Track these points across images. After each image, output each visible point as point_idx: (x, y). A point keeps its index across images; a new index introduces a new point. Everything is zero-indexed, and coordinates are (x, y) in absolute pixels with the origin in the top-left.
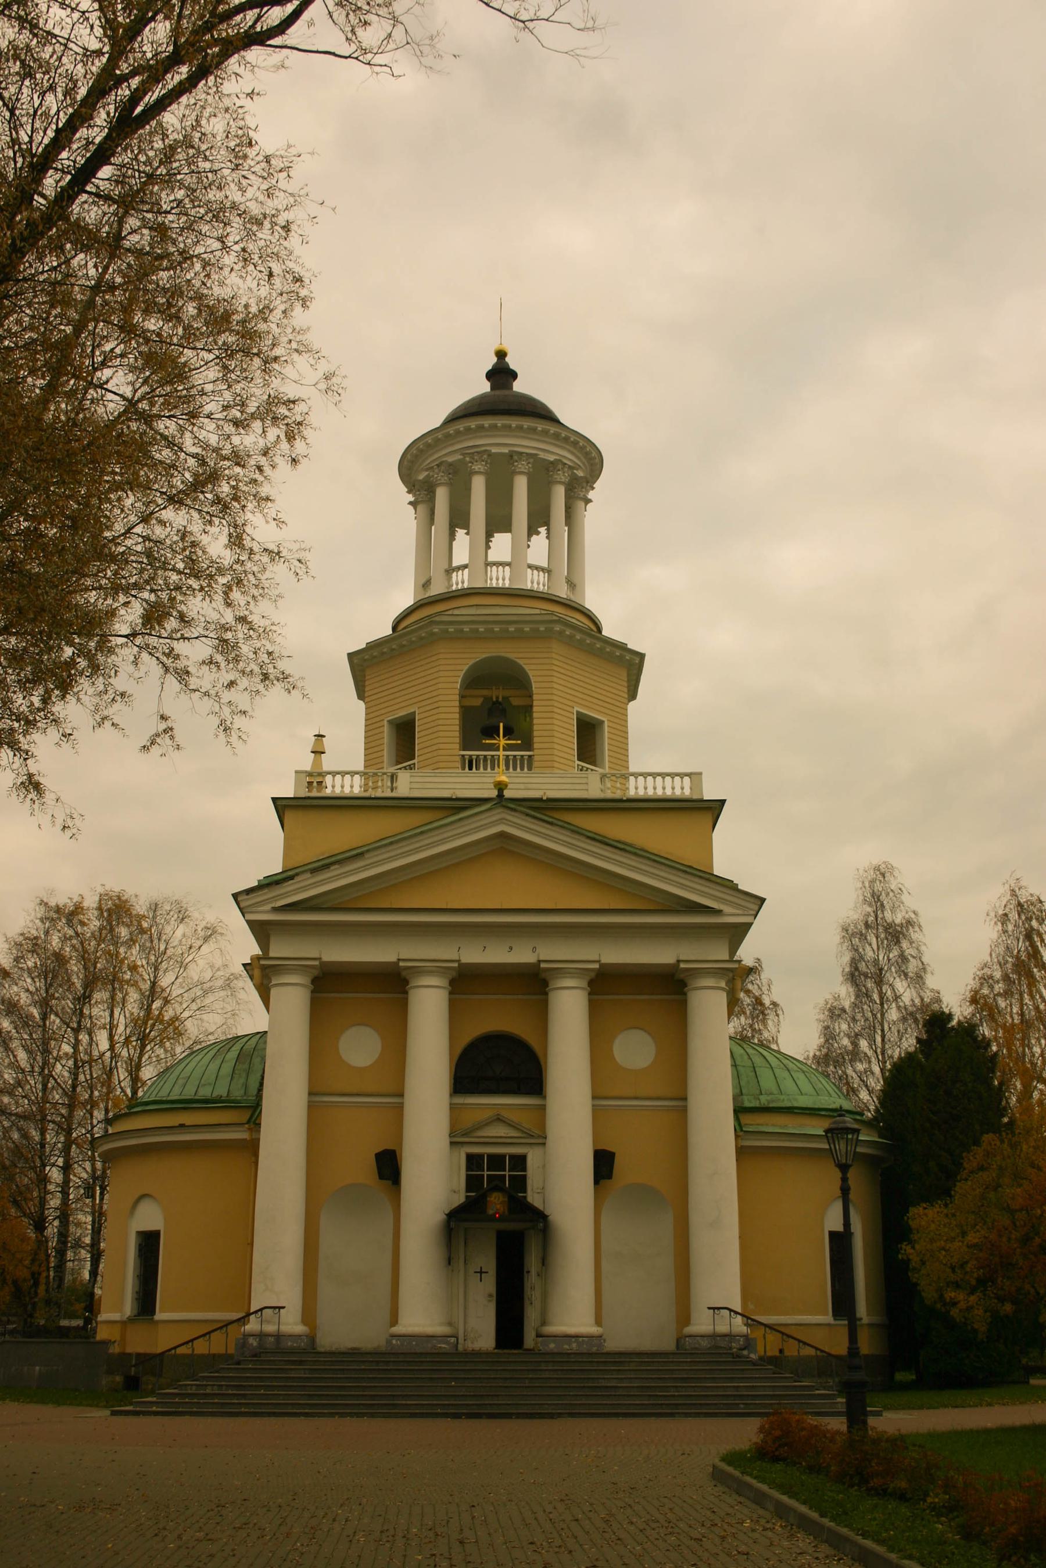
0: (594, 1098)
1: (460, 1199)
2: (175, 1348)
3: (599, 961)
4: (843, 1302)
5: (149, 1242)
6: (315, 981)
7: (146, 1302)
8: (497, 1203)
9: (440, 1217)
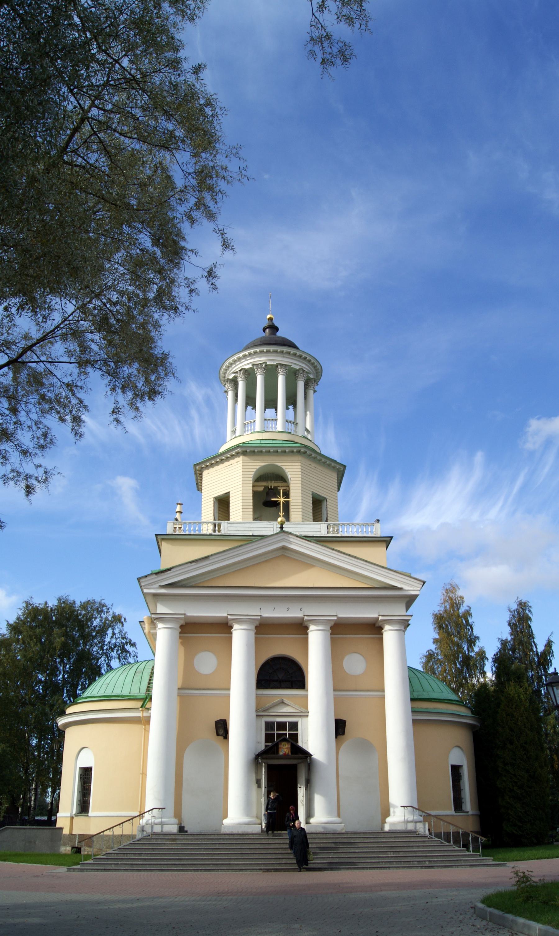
0: (334, 690)
1: (262, 747)
2: (103, 832)
3: (336, 616)
4: (458, 804)
5: (86, 774)
6: (182, 627)
7: (84, 807)
8: (285, 749)
9: (254, 756)
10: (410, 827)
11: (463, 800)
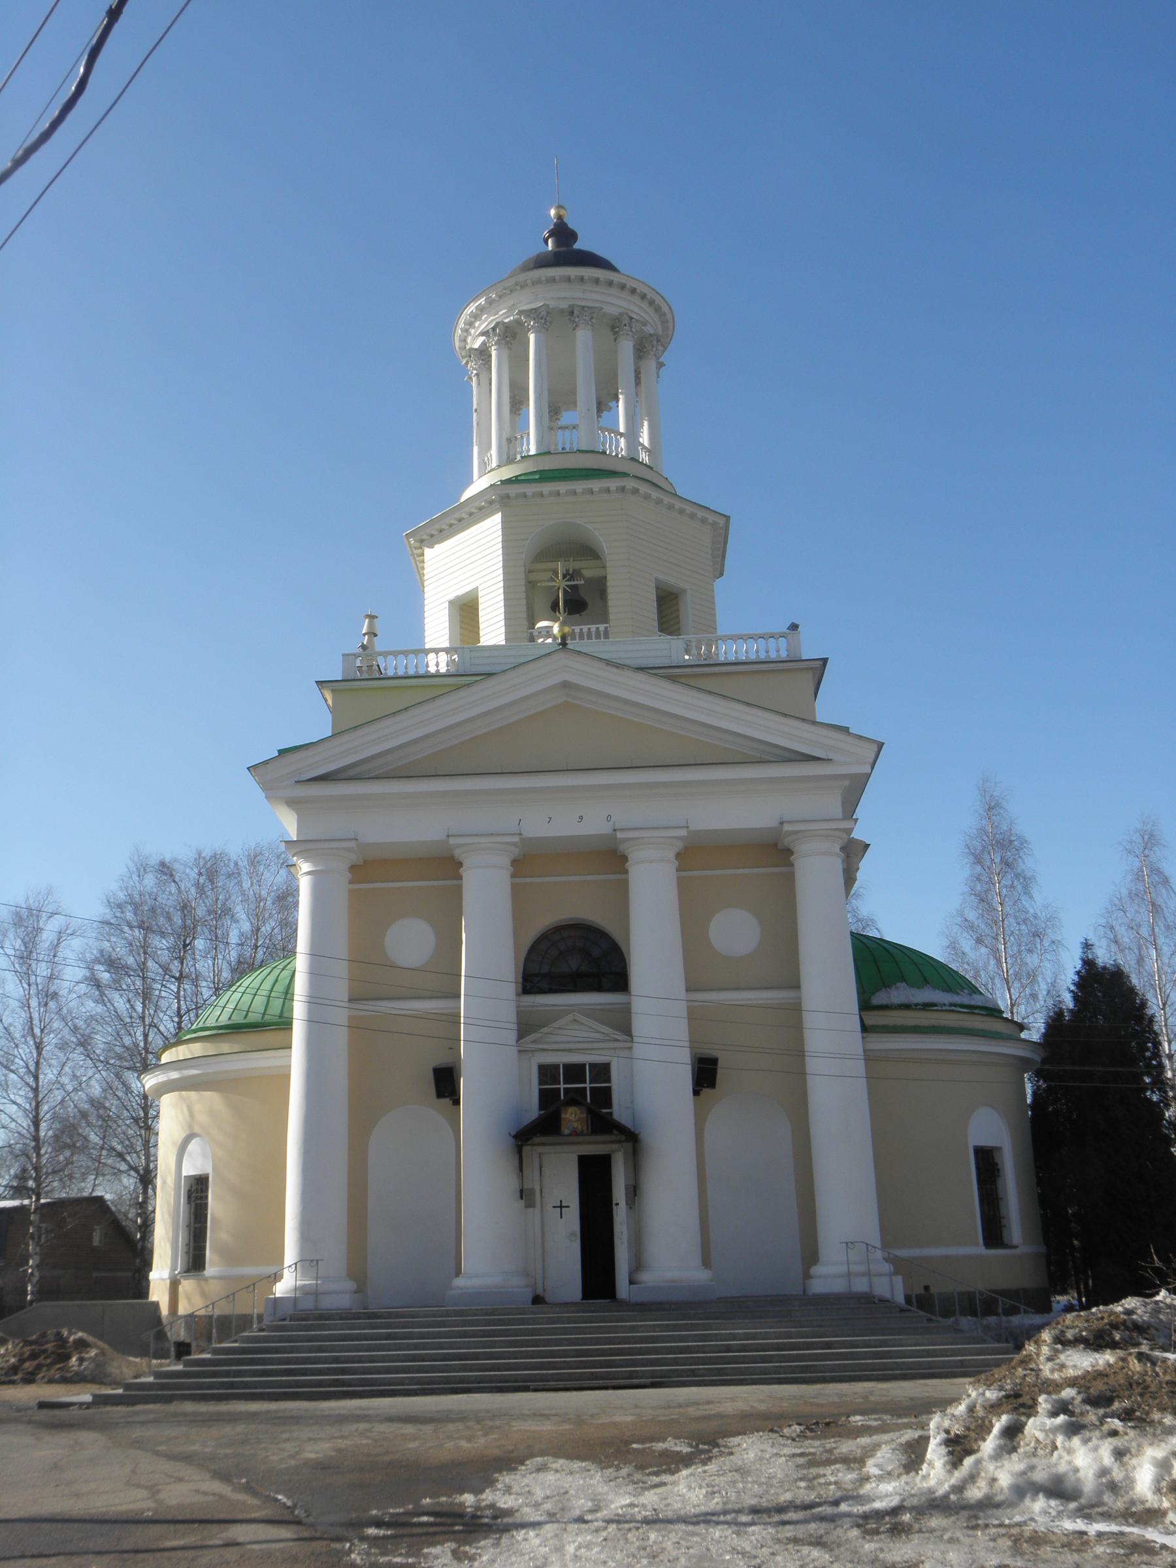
0: (688, 990)
1: (533, 1111)
4: (993, 1233)
8: (572, 1117)
10: (860, 1286)
11: (1004, 1222)
